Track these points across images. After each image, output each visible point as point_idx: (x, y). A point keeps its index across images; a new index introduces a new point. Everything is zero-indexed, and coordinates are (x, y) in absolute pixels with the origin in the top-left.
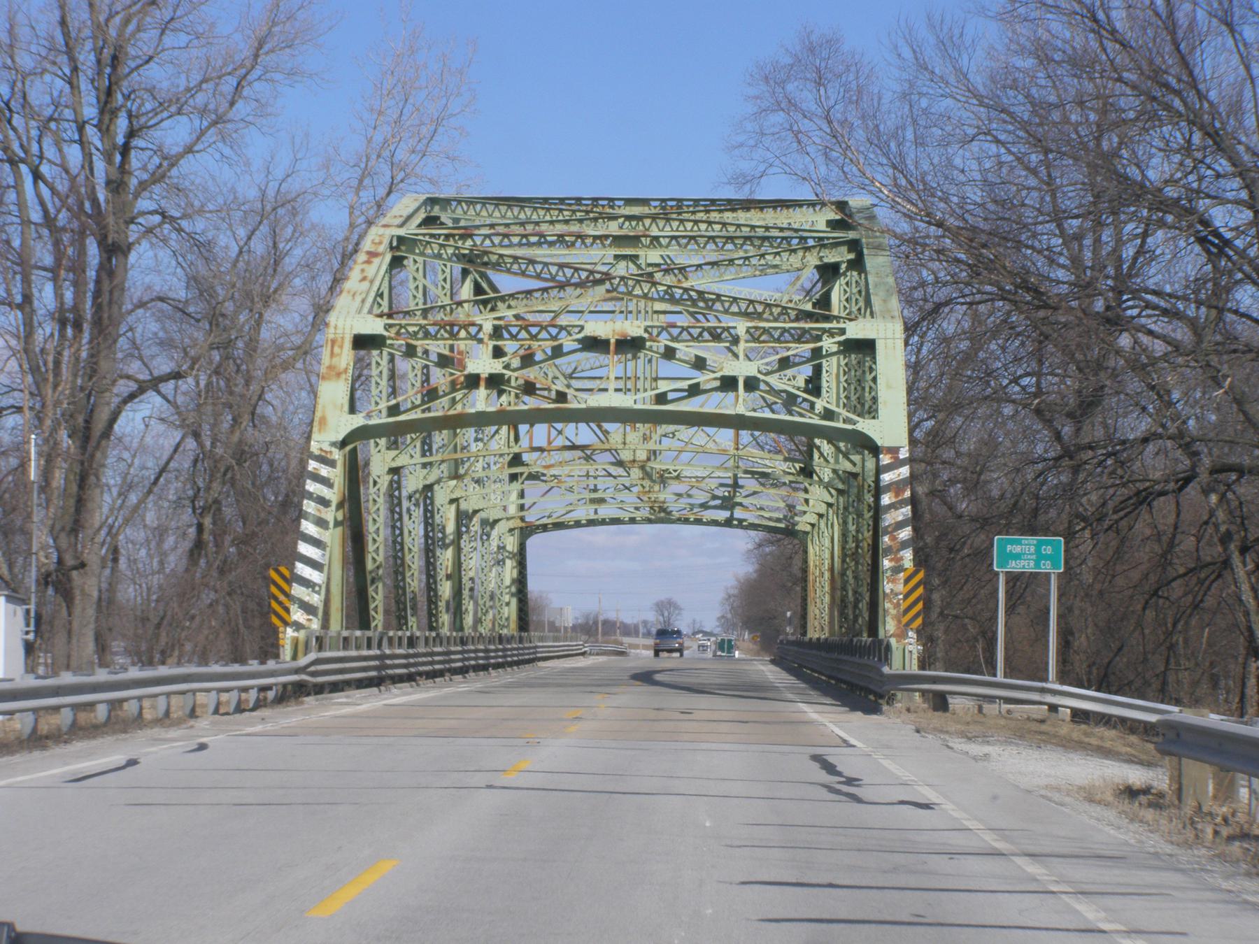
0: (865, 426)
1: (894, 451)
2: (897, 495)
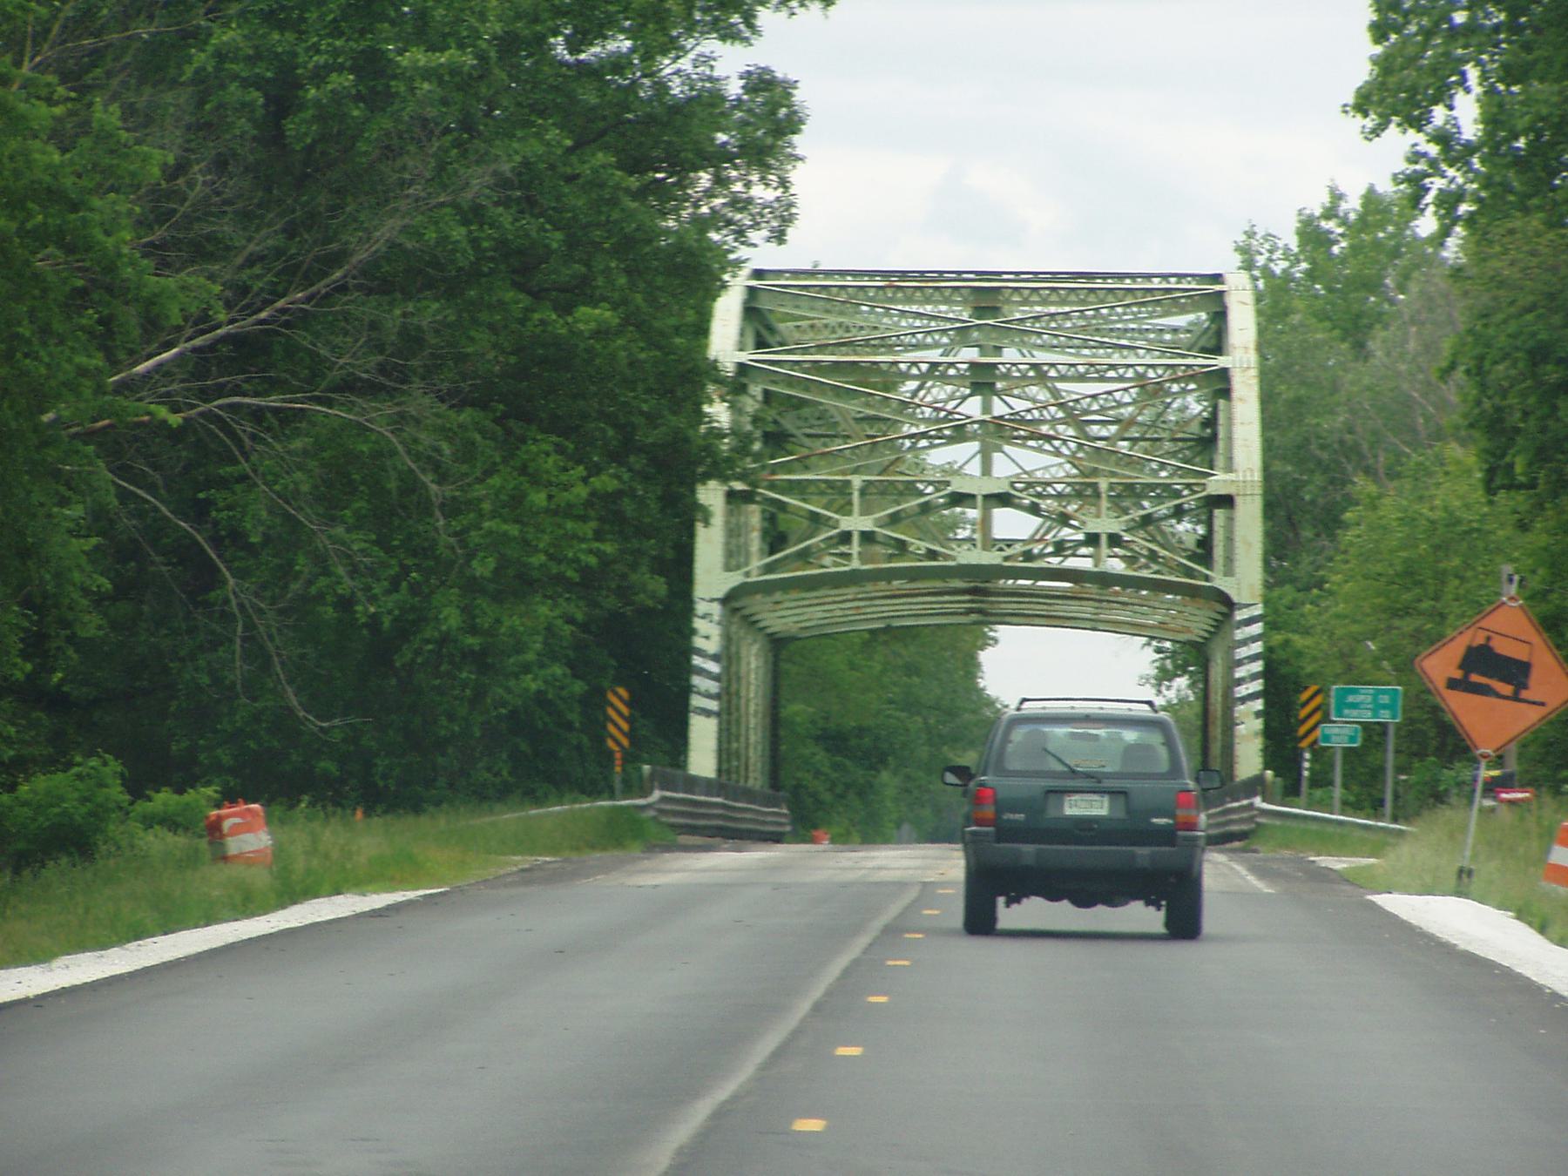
0: (1220, 582)
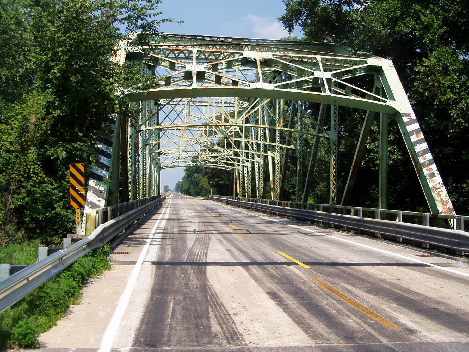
1: (408, 115)
2: (417, 136)
